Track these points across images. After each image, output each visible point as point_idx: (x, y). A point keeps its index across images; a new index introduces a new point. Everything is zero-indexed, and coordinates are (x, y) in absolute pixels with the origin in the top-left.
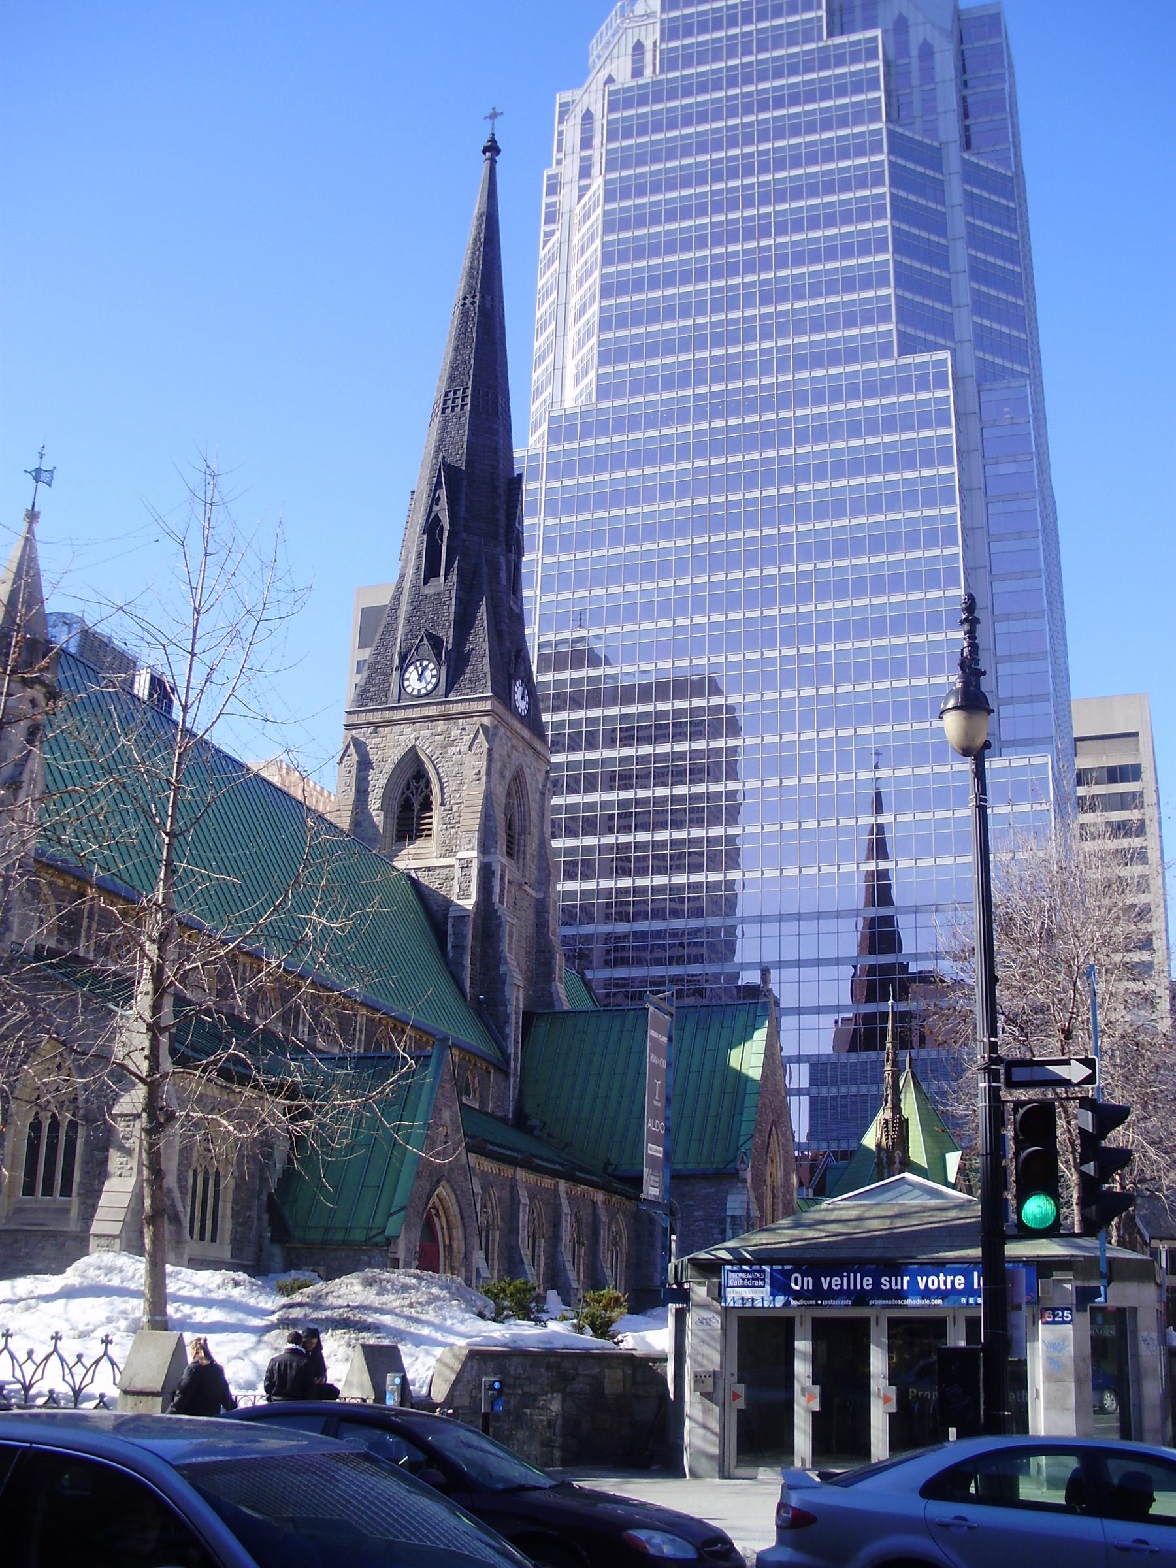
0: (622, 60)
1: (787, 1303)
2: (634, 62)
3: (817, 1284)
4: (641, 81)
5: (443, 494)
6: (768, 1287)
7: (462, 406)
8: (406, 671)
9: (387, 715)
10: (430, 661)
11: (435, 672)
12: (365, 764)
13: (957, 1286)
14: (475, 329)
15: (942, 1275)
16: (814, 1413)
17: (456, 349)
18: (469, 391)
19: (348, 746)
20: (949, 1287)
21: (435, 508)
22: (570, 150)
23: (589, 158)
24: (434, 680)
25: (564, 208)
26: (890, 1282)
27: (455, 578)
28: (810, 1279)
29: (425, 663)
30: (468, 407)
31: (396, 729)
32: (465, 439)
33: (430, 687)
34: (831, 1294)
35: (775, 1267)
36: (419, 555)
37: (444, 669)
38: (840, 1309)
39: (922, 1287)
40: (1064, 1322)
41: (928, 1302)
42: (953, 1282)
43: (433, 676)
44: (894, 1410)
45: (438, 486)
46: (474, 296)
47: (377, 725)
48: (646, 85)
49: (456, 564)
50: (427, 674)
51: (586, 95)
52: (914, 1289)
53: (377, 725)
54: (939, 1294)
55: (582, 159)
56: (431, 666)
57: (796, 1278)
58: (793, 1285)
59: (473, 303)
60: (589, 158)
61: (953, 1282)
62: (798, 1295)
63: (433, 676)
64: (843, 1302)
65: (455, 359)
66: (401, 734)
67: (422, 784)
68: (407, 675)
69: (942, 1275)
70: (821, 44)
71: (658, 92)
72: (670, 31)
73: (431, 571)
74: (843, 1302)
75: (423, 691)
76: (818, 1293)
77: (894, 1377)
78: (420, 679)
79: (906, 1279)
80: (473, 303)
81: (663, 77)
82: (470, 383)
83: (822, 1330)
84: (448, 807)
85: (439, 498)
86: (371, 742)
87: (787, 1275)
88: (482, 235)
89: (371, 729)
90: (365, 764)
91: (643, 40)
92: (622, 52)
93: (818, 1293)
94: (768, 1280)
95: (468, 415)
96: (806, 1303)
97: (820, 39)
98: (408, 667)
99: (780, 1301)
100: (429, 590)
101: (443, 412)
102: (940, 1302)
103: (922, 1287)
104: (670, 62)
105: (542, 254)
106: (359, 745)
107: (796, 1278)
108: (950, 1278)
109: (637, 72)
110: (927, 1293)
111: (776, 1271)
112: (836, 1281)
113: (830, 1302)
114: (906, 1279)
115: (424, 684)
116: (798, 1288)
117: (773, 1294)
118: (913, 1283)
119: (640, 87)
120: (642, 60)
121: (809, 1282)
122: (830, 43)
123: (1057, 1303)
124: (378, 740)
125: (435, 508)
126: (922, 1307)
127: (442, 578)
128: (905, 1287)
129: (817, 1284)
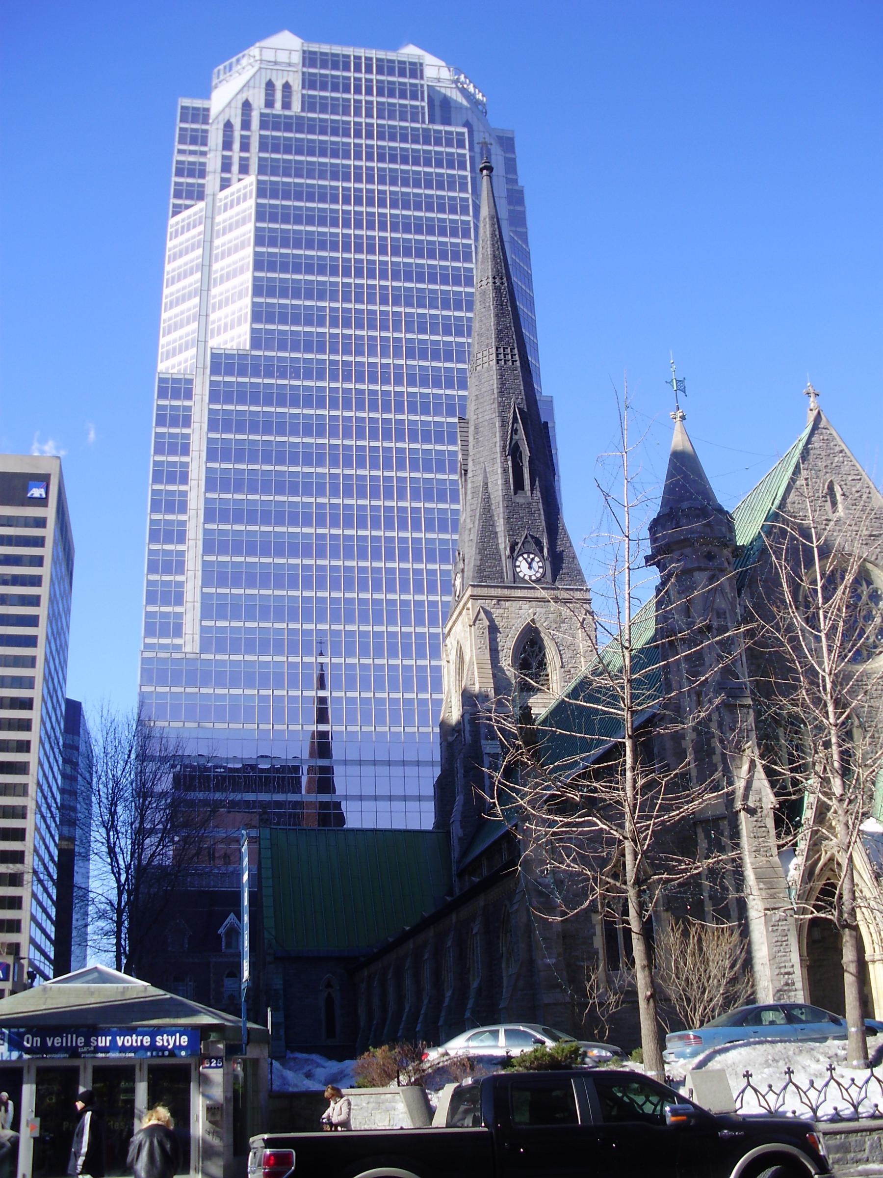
0: (257, 90)
1: (20, 1057)
2: (267, 95)
3: (44, 1042)
4: (287, 113)
5: (520, 426)
6: (6, 1045)
7: (513, 362)
8: (517, 560)
9: (506, 592)
10: (536, 555)
11: (540, 564)
12: (493, 629)
13: (145, 1043)
14: (509, 304)
15: (165, 1035)
16: (35, 1139)
17: (497, 316)
18: (516, 351)
19: (479, 612)
20: (139, 1044)
21: (515, 437)
22: (213, 147)
23: (230, 158)
24: (541, 570)
25: (208, 191)
26: (97, 1041)
27: (539, 494)
28: (39, 1039)
29: (532, 556)
30: (518, 363)
31: (515, 604)
32: (522, 388)
33: (538, 575)
34: (54, 1050)
35: (13, 1030)
36: (505, 471)
37: (548, 563)
38: (60, 1060)
39: (120, 1044)
40: (217, 1067)
41: (123, 1055)
42: (142, 1041)
43: (540, 567)
44: (37, 1135)
45: (515, 419)
46: (501, 279)
47: (500, 599)
48: (290, 117)
49: (537, 483)
50: (535, 565)
51: (227, 109)
52: (113, 1046)
53: (500, 599)
54: (132, 1049)
55: (224, 157)
56: (537, 559)
57: (28, 1039)
58: (25, 1043)
59: (502, 283)
60: (230, 158)
61: (142, 1041)
62: (28, 1051)
63: (540, 567)
64: (62, 1056)
65: (498, 324)
66: (520, 608)
67: (536, 648)
68: (518, 563)
69: (165, 1035)
70: (424, 126)
71: (299, 124)
72: (309, 82)
73: (519, 485)
74: (62, 1056)
75: (533, 578)
76: (44, 1049)
77: (39, 1111)
78: (530, 568)
79: (109, 1038)
80: (502, 283)
81: (304, 114)
82: (515, 345)
83: (43, 1077)
84: (566, 669)
85: (516, 430)
86: (496, 613)
87: (21, 1036)
88: (497, 233)
89: (494, 602)
90: (493, 629)
91: (274, 80)
92: (257, 85)
93: (44, 1049)
94: (6, 1039)
95: (519, 369)
96: (35, 1056)
97: (423, 122)
98: (518, 557)
99: (15, 1055)
100: (520, 499)
101: (498, 363)
102: (133, 1055)
103: (120, 1044)
104: (309, 104)
105: (172, 221)
106: (488, 614)
107: (28, 1039)
108: (140, 1038)
109: (269, 104)
110: (123, 1049)
111: (13, 1033)
112: (57, 1041)
113: (53, 1056)
114: (109, 1038)
115: (532, 572)
116: (29, 1045)
117: (10, 1050)
118: (114, 1041)
119: (286, 117)
120: (273, 95)
121: (37, 1041)
122: (430, 127)
123: (213, 1054)
124: (501, 611)
125: (515, 437)
126: (120, 1059)
127: (529, 494)
128: (108, 1044)
129: (44, 1042)
